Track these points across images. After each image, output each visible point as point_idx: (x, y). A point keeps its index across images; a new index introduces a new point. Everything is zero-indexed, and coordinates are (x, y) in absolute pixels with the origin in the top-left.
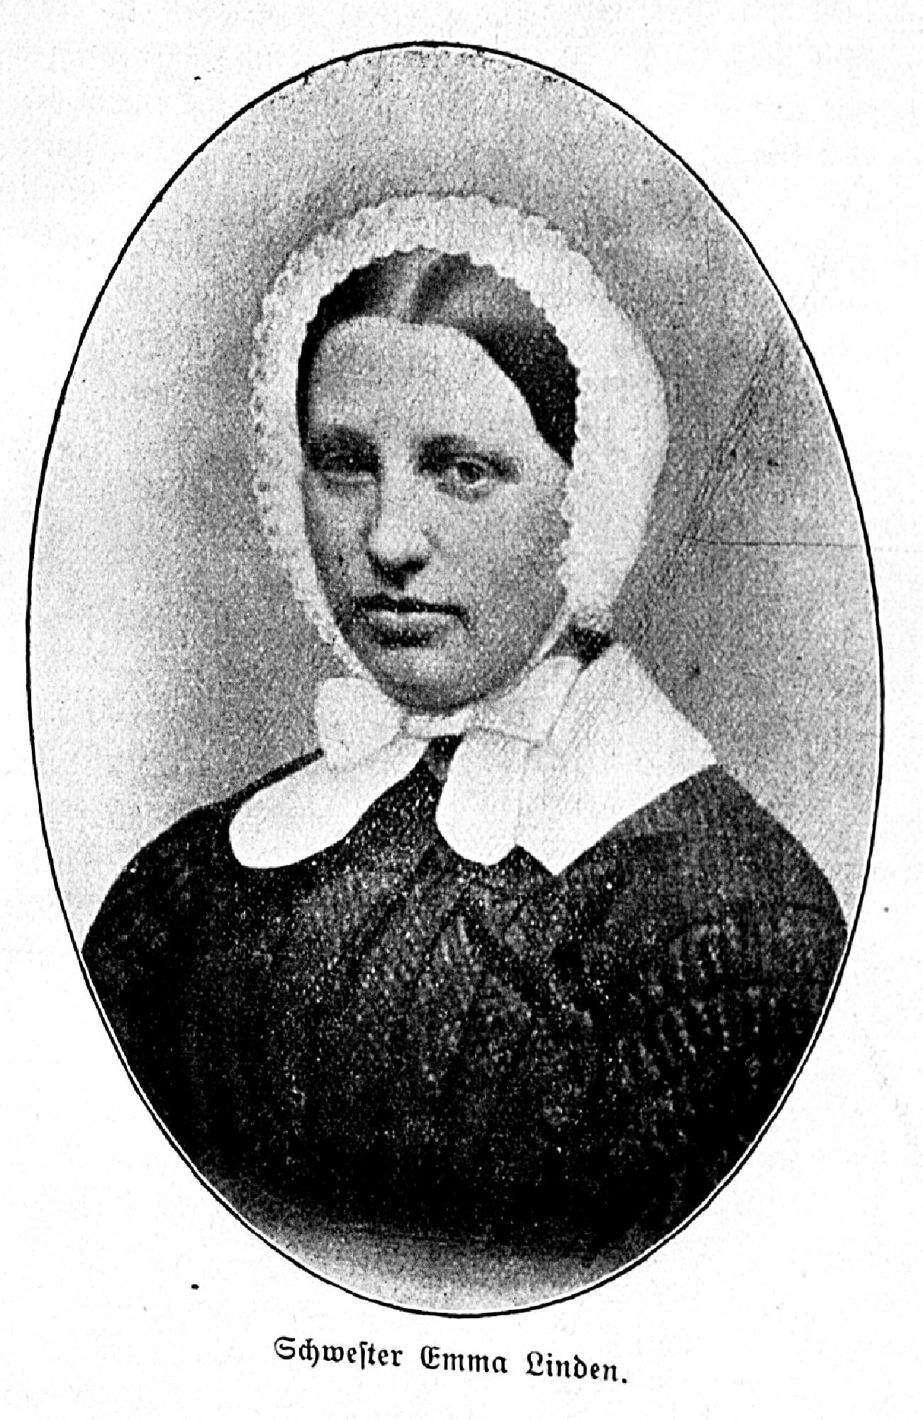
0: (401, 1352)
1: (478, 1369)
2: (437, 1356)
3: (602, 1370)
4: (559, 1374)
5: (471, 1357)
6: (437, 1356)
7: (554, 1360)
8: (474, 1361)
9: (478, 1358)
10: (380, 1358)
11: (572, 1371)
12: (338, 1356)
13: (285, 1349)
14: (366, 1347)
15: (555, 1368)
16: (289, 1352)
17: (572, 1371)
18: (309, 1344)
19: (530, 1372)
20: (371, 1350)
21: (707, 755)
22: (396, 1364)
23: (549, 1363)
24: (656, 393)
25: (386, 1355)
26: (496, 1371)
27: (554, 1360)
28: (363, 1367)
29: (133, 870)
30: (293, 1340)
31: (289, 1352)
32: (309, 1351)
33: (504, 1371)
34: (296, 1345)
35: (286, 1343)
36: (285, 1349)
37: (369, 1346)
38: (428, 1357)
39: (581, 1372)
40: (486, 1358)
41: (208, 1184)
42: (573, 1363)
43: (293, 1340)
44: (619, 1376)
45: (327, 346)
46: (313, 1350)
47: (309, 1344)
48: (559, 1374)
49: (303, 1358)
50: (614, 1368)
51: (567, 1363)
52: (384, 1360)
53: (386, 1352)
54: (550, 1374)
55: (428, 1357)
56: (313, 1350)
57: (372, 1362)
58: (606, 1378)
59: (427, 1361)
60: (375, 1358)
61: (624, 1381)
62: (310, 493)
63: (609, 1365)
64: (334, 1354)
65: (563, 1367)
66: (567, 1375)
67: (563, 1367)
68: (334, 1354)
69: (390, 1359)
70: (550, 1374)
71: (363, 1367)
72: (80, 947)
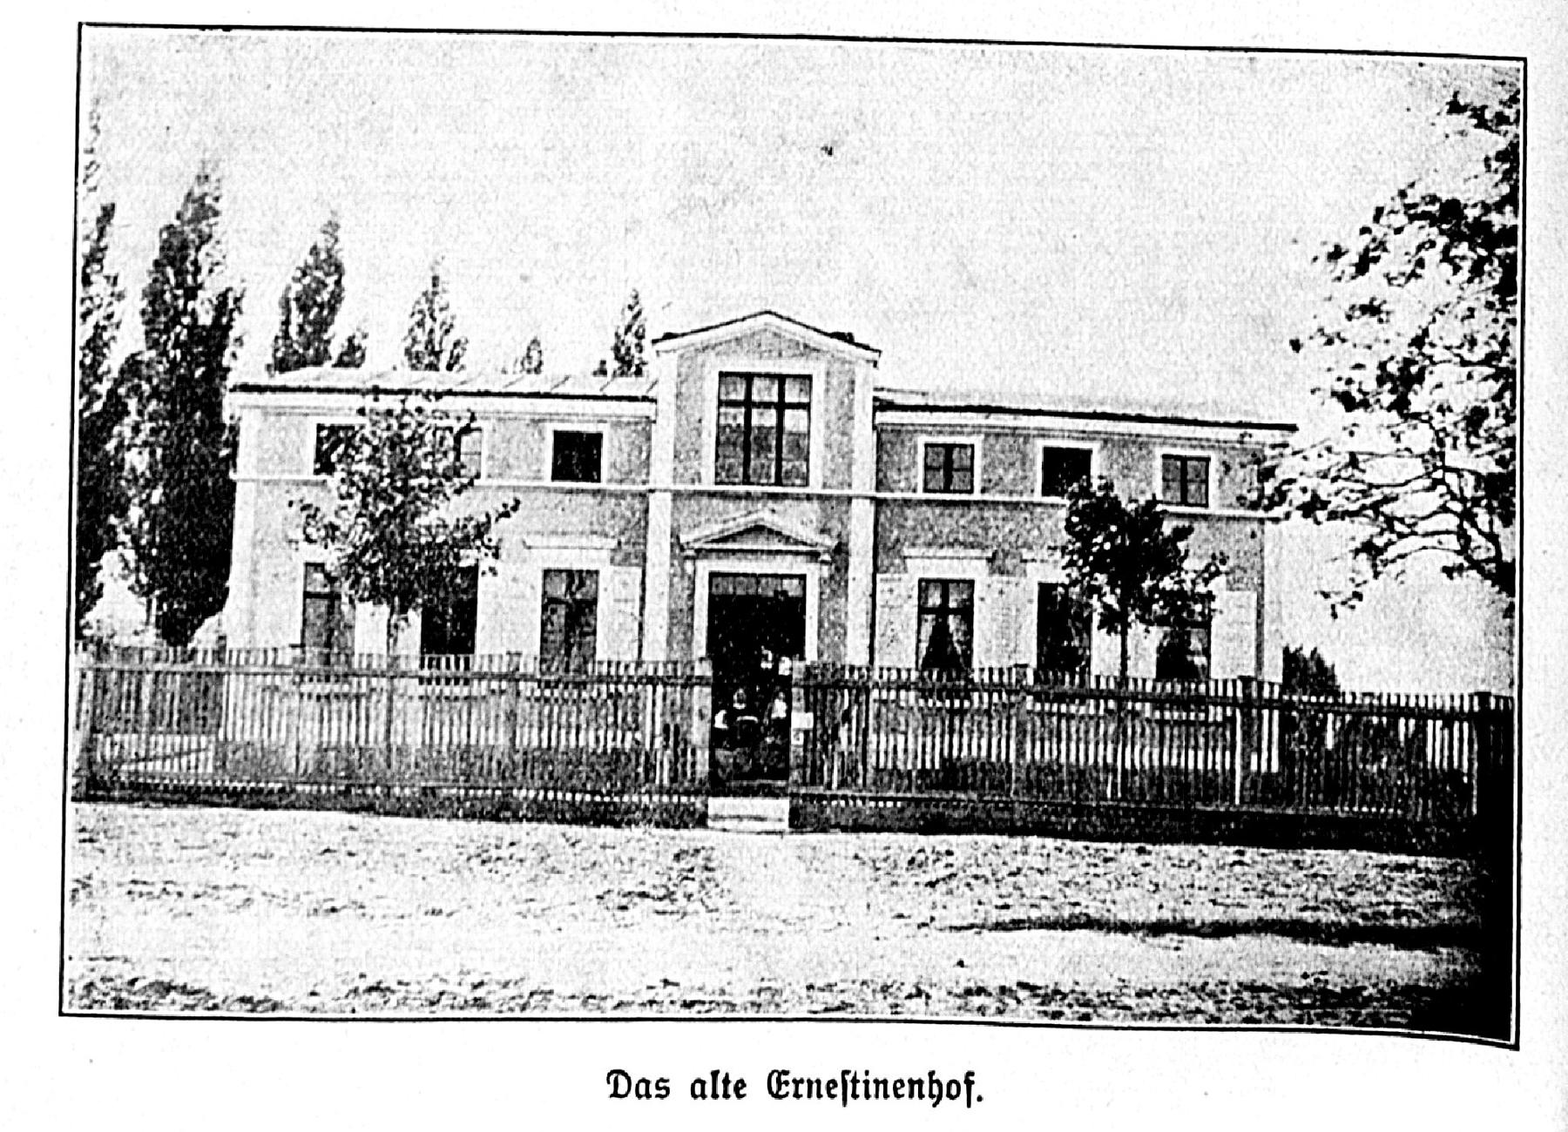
2: (787, 1083)
6: (787, 1083)
7: (871, 1078)
10: (895, 1089)
11: (926, 1091)
14: (849, 1078)
19: (615, 1094)
20: (726, 1081)
23: (867, 1082)
27: (733, 1079)
28: (969, 1105)
38: (778, 1083)
40: (885, 1082)
48: (809, 1096)
49: (639, 1096)
52: (900, 1092)
53: (901, 1081)
55: (778, 1083)
57: (855, 1096)
59: (774, 1089)
62: (625, 420)
65: (815, 1086)
66: (819, 1096)
67: (815, 1086)
71: (969, 1105)
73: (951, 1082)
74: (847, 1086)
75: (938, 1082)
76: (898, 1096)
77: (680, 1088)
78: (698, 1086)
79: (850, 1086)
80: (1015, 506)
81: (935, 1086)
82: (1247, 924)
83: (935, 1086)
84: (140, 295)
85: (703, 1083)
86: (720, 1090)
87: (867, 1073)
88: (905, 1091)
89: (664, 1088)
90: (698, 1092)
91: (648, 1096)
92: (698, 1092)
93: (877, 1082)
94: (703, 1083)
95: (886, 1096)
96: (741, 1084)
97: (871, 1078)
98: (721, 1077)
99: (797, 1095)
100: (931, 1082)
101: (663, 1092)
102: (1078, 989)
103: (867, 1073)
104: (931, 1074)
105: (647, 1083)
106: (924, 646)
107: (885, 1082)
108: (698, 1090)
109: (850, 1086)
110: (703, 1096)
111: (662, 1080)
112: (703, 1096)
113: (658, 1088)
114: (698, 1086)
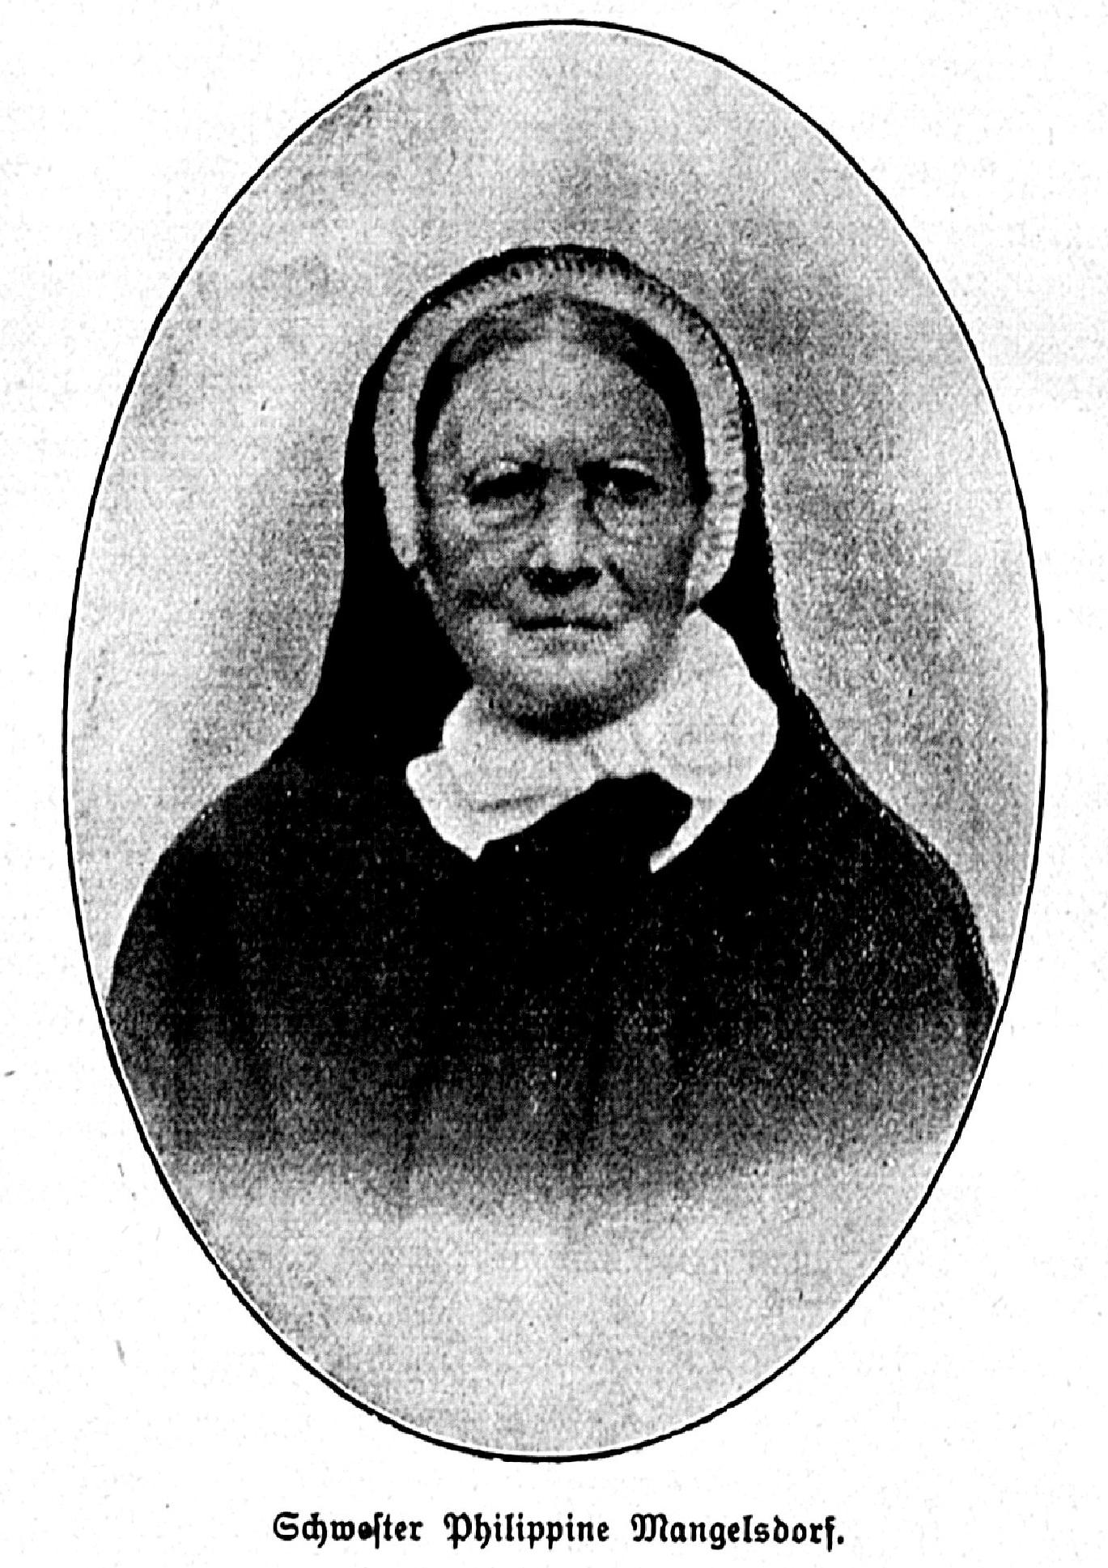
0: (420, 1524)
4: (694, 1539)
10: (398, 1532)
12: (347, 1532)
13: (285, 1527)
15: (576, 1531)
16: (291, 1532)
18: (315, 1520)
20: (388, 1524)
22: (415, 1537)
27: (394, 1521)
30: (295, 1516)
31: (291, 1532)
32: (315, 1529)
34: (299, 1523)
35: (287, 1521)
36: (285, 1527)
39: (781, 1534)
40: (702, 1525)
41: (154, 1149)
42: (772, 1526)
43: (295, 1516)
45: (465, 393)
46: (320, 1528)
47: (315, 1520)
48: (694, 1539)
56: (320, 1528)
57: (388, 1537)
59: (282, 1520)
63: (697, 1523)
64: (344, 1531)
67: (698, 1530)
68: (344, 1531)
69: (408, 1532)
71: (377, 1546)
72: (103, 991)
73: (677, 1525)
75: (486, 1524)
76: (401, 1538)
80: (731, 362)
81: (483, 1529)
83: (483, 1529)
86: (515, 1532)
87: (570, 1516)
90: (555, 1529)
92: (555, 1529)
93: (581, 1525)
95: (591, 1538)
96: (604, 1527)
98: (515, 1521)
99: (815, 1540)
100: (479, 1524)
102: (326, 1289)
103: (570, 1516)
106: (914, 839)
107: (590, 1525)
110: (683, 1539)
112: (683, 1539)
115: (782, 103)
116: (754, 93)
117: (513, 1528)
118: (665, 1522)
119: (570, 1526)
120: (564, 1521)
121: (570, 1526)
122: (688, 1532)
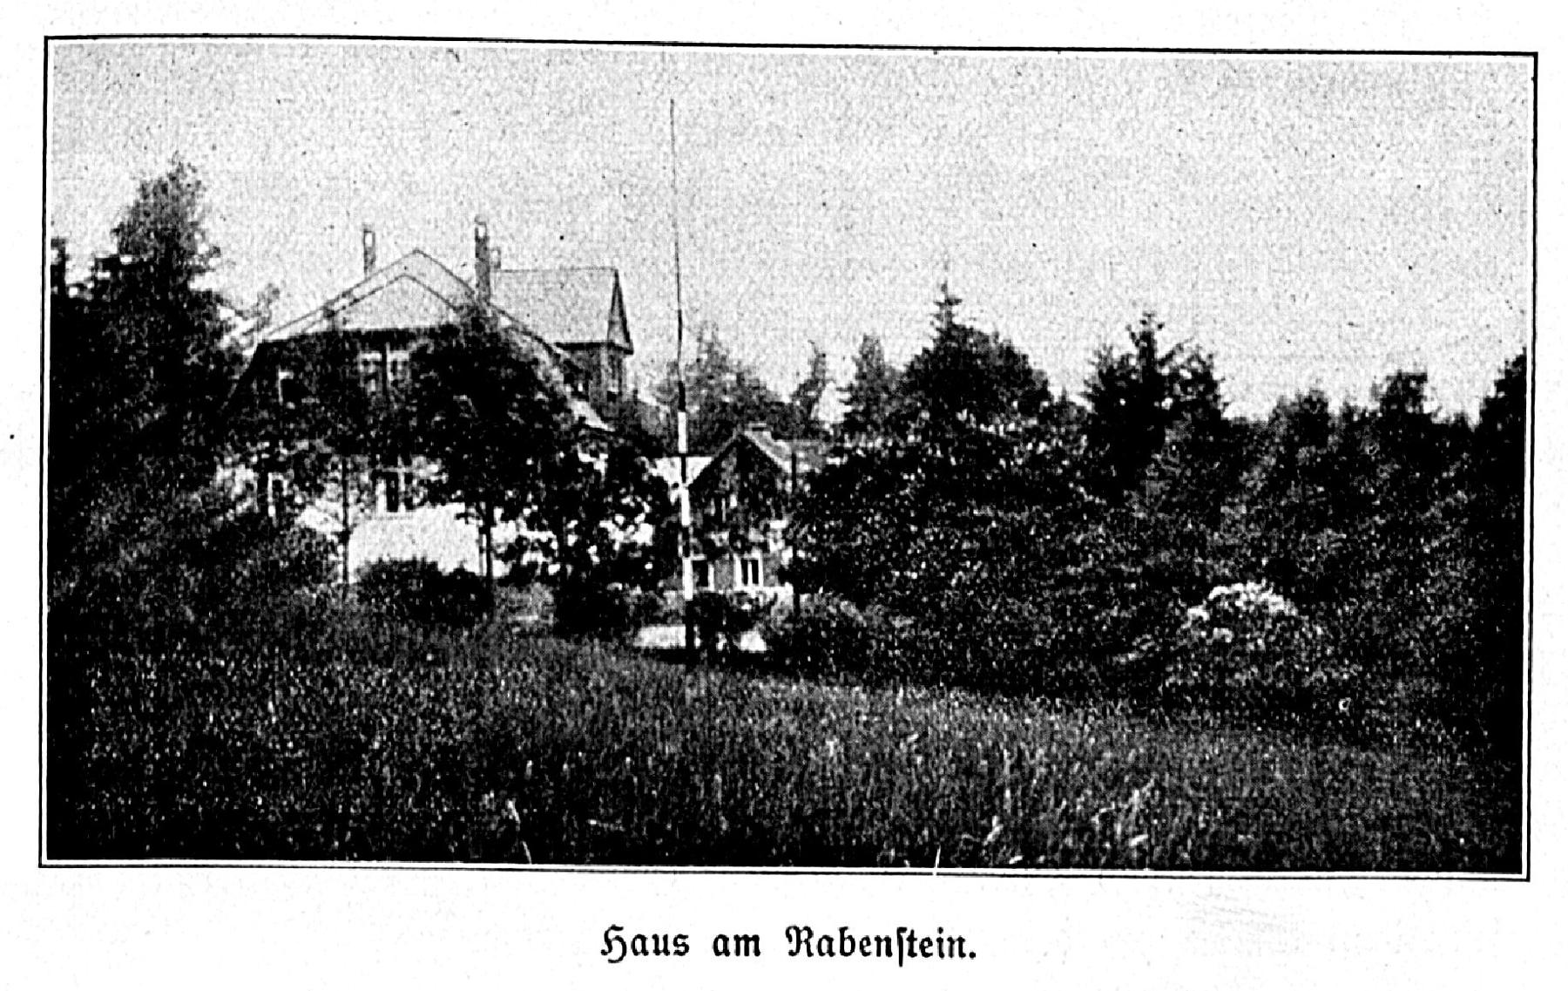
1: (747, 954)
3: (874, 944)
4: (738, 953)
5: (737, 938)
8: (742, 943)
9: (746, 938)
10: (922, 948)
11: (836, 947)
14: (905, 936)
17: (836, 947)
20: (911, 939)
21: (1342, 396)
24: (721, 336)
25: (931, 944)
26: (821, 954)
27: (919, 936)
29: (545, 522)
33: (757, 953)
37: (908, 933)
38: (799, 937)
39: (847, 948)
44: (966, 950)
48: (738, 953)
50: (756, 939)
51: (888, 940)
52: (867, 949)
53: (928, 939)
54: (942, 955)
57: (912, 954)
58: (879, 954)
60: (917, 949)
61: (973, 955)
63: (955, 937)
65: (661, 947)
67: (883, 944)
70: (942, 955)
74: (845, 944)
75: (850, 937)
77: (701, 945)
78: (721, 942)
79: (906, 945)
82: (332, 351)
84: (107, 228)
85: (830, 940)
87: (941, 930)
88: (873, 948)
89: (683, 950)
90: (721, 948)
91: (667, 952)
92: (721, 948)
94: (830, 940)
97: (944, 936)
100: (842, 939)
101: (682, 949)
103: (941, 930)
104: (842, 930)
105: (643, 938)
108: (721, 947)
109: (906, 945)
110: (727, 953)
111: (614, 928)
112: (727, 953)
113: (676, 944)
114: (721, 942)
115: (1454, 57)
116: (984, 61)
117: (845, 944)
118: (810, 934)
119: (940, 941)
120: (934, 937)
121: (940, 941)
122: (732, 945)
